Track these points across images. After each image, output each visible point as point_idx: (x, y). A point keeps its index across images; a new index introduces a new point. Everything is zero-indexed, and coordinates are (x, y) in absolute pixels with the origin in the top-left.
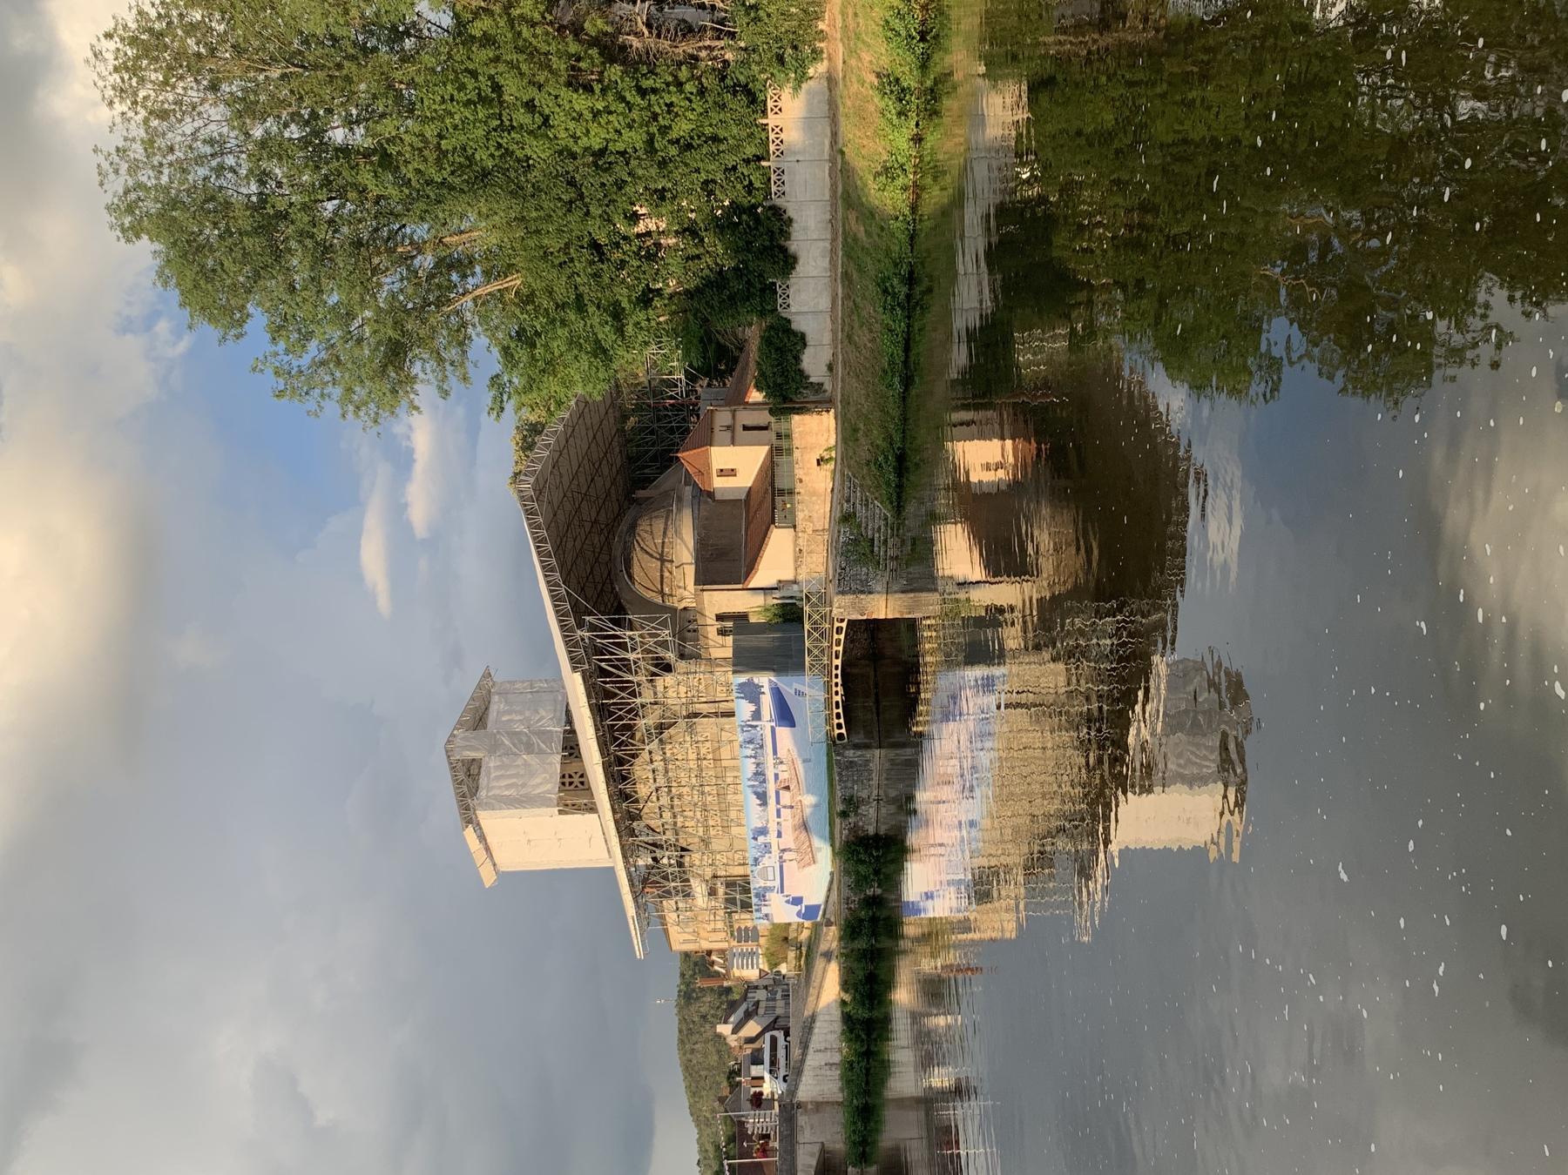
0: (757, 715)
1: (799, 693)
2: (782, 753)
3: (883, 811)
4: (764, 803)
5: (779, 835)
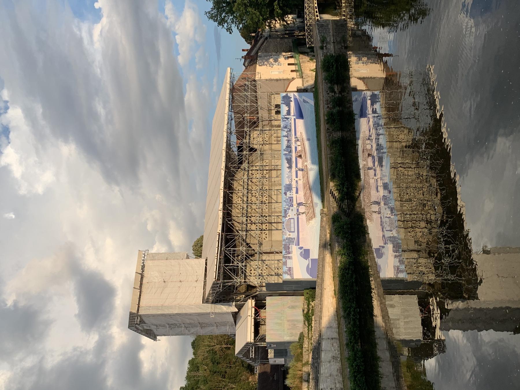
0: (289, 113)
1: (305, 101)
2: (298, 135)
3: (336, 47)
4: (290, 167)
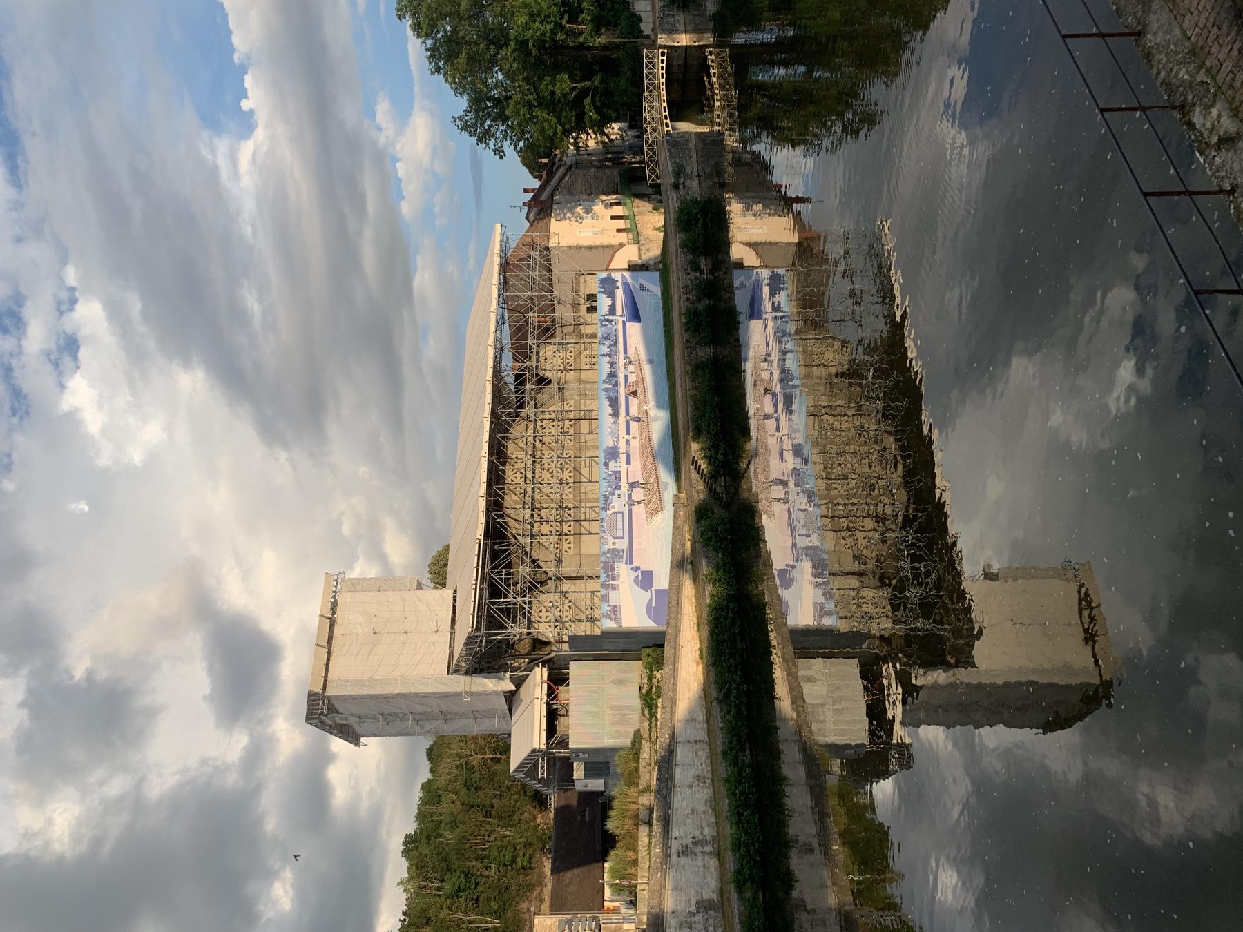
0: (612, 310)
2: (631, 352)
3: (703, 185)
4: (615, 414)
5: (628, 462)
